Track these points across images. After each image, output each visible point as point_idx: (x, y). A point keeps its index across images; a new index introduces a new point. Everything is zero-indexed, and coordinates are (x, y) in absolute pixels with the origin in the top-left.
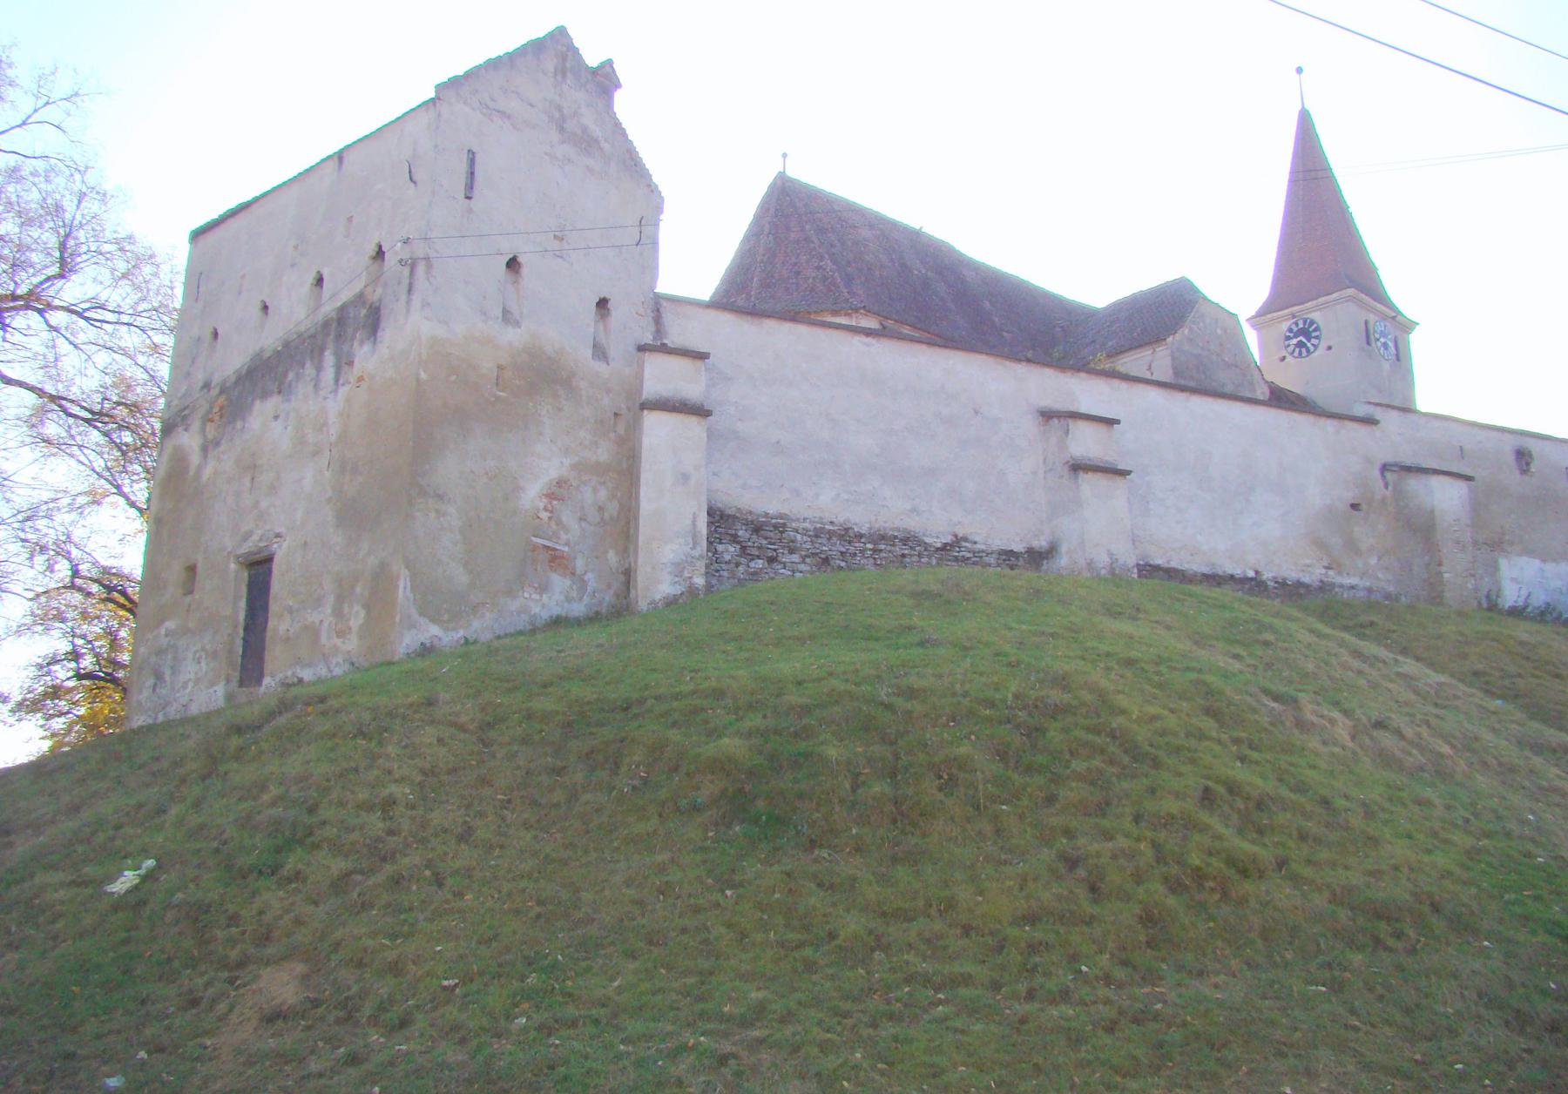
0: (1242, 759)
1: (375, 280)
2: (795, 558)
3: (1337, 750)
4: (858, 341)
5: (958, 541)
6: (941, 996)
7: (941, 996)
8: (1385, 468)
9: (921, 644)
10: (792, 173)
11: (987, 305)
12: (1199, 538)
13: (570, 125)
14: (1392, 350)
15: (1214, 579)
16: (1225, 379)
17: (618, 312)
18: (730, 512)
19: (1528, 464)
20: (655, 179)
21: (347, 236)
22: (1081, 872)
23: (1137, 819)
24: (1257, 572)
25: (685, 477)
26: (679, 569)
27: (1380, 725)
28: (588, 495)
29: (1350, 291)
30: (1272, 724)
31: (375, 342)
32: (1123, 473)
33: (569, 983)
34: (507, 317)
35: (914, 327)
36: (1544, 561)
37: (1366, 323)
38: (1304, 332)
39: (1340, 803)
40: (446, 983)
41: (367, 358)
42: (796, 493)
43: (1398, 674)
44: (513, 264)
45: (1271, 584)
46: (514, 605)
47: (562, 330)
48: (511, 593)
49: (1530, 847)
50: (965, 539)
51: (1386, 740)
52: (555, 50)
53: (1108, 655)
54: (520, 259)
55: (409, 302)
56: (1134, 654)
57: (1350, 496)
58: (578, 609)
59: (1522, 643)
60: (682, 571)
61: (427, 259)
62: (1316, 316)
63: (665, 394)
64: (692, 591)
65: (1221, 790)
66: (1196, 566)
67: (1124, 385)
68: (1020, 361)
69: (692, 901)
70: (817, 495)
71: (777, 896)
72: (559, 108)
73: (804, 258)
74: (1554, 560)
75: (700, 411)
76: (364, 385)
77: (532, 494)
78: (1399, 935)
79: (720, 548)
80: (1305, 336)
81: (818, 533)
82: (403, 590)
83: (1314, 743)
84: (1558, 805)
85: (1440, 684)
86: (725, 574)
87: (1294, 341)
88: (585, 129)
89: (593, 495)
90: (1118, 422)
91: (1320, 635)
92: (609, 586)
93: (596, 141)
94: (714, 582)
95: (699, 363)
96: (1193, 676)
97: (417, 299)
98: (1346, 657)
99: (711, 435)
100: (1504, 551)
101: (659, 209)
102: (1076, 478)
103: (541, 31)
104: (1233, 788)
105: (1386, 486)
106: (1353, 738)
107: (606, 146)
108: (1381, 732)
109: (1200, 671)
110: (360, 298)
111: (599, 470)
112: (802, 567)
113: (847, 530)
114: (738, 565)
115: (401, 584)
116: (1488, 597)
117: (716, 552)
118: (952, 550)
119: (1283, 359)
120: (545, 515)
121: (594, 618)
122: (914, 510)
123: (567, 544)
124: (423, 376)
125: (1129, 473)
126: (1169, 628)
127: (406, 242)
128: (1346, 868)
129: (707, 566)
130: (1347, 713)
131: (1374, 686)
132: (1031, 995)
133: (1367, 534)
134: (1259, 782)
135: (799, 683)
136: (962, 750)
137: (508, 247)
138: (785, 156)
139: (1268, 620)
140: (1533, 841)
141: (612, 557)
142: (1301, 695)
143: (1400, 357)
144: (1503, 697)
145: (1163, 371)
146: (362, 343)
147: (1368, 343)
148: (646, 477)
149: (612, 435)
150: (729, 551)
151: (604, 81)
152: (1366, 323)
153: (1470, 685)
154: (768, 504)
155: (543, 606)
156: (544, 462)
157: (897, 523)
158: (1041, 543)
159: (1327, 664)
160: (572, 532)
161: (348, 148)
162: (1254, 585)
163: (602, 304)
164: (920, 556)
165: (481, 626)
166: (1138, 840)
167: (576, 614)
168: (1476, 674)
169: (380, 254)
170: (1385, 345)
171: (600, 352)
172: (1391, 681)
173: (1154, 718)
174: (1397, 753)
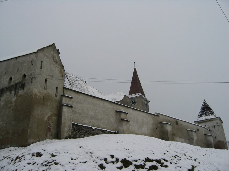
1: (23, 80)
21: (18, 71)
26: (67, 132)
34: (45, 89)
44: (46, 80)
47: (52, 92)
54: (47, 79)
61: (35, 78)
88: (56, 60)
110: (20, 82)
143: (147, 106)
163: (57, 88)
169: (25, 76)
171: (56, 96)
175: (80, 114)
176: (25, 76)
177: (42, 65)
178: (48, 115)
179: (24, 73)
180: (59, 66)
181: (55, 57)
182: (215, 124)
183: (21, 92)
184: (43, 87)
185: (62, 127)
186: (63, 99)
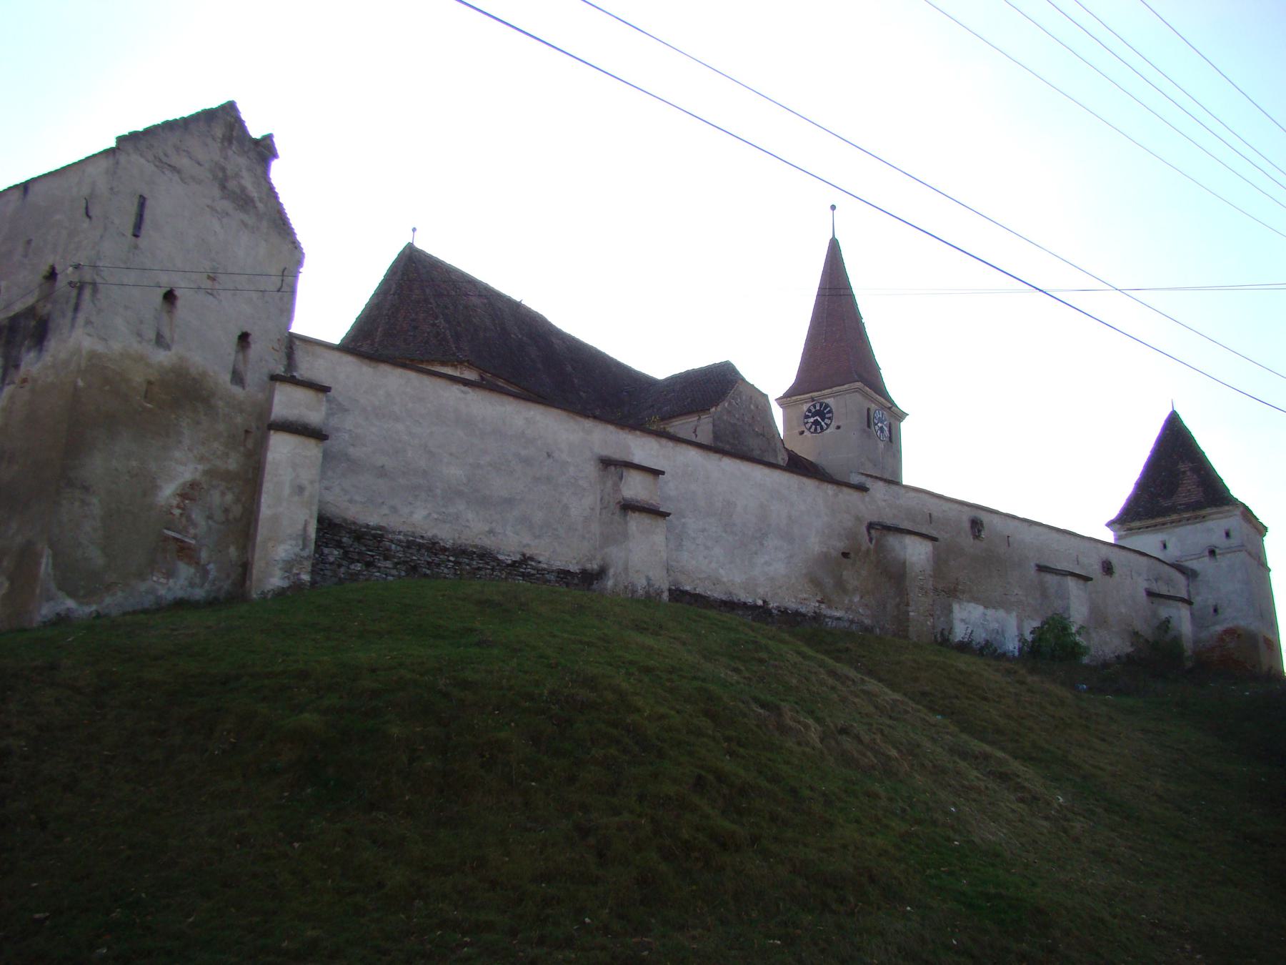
0: (732, 753)
1: (47, 296)
2: (388, 564)
3: (807, 750)
4: (455, 391)
5: (525, 559)
6: (467, 939)
7: (467, 939)
8: (871, 526)
9: (479, 644)
10: (419, 245)
11: (569, 368)
12: (721, 571)
13: (232, 185)
14: (887, 433)
15: (730, 605)
17: (256, 348)
18: (337, 521)
19: (979, 531)
20: (299, 238)
21: (26, 256)
22: (592, 840)
23: (641, 798)
24: (764, 602)
25: (300, 489)
26: (288, 566)
27: (844, 731)
28: (216, 498)
29: (859, 384)
30: (757, 726)
31: (40, 350)
32: (664, 515)
33: (149, 918)
34: (160, 341)
35: (507, 381)
36: (986, 607)
38: (820, 413)
39: (806, 793)
40: (37, 916)
41: (32, 364)
42: (394, 509)
43: (863, 691)
44: (170, 297)
45: (775, 612)
46: (143, 587)
48: (141, 576)
49: (951, 834)
50: (531, 559)
51: (848, 744)
52: (223, 122)
53: (631, 663)
54: (177, 293)
55: (74, 319)
56: (651, 663)
57: (841, 545)
58: (199, 593)
59: (961, 672)
60: (291, 568)
61: (94, 284)
62: (830, 401)
63: (291, 418)
64: (297, 587)
65: (711, 777)
66: (717, 593)
67: (671, 444)
68: (587, 417)
69: (265, 851)
70: (412, 513)
71: (338, 849)
72: (223, 169)
73: (422, 316)
74: (994, 608)
75: (317, 434)
76: (28, 386)
77: (168, 492)
78: (842, 900)
79: (326, 551)
80: (820, 416)
81: (409, 545)
82: (45, 565)
83: (790, 743)
84: (975, 800)
85: (895, 701)
86: (328, 573)
87: (812, 420)
88: (243, 189)
89: (219, 498)
90: (663, 473)
91: (804, 656)
92: (228, 576)
93: (252, 201)
94: (318, 579)
95: (321, 395)
96: (697, 684)
97: (81, 317)
98: (823, 675)
99: (327, 456)
100: (956, 597)
101: (299, 262)
102: (625, 515)
103: (214, 103)
104: (720, 777)
105: (871, 540)
106: (822, 741)
107: (259, 205)
108: (844, 737)
109: (704, 680)
110: (31, 312)
111: (227, 476)
112: (394, 572)
113: (434, 544)
114: (340, 566)
115: (44, 561)
116: (942, 634)
117: (322, 554)
118: (522, 566)
119: (802, 433)
120: (177, 512)
121: (212, 603)
122: (491, 532)
123: (195, 537)
124: (81, 383)
125: (668, 514)
126: (684, 644)
127: (77, 267)
128: (805, 845)
129: (313, 565)
130: (819, 720)
131: (843, 700)
132: (541, 941)
133: (852, 578)
134: (742, 772)
135: (374, 671)
136: (502, 735)
137: (166, 281)
139: (764, 641)
140: (952, 827)
141: (233, 551)
142: (783, 704)
143: (893, 441)
144: (943, 713)
145: (705, 436)
146: (29, 350)
147: (869, 426)
148: (268, 486)
149: (242, 449)
150: (334, 554)
151: (264, 150)
153: (918, 703)
154: (373, 518)
155: (169, 589)
156: (180, 469)
157: (477, 542)
158: (594, 566)
159: (807, 679)
160: (200, 527)
161: (33, 180)
162: (761, 613)
163: (244, 338)
164: (493, 569)
165: (113, 602)
166: (640, 816)
167: (197, 597)
168: (924, 694)
169: (52, 275)
170: (881, 429)
171: (238, 378)
172: (857, 696)
173: (662, 717)
174: (856, 754)
176: (52, 275)
178: (181, 481)
180: (265, 223)
181: (237, 176)
182: (1217, 539)
185: (259, 539)
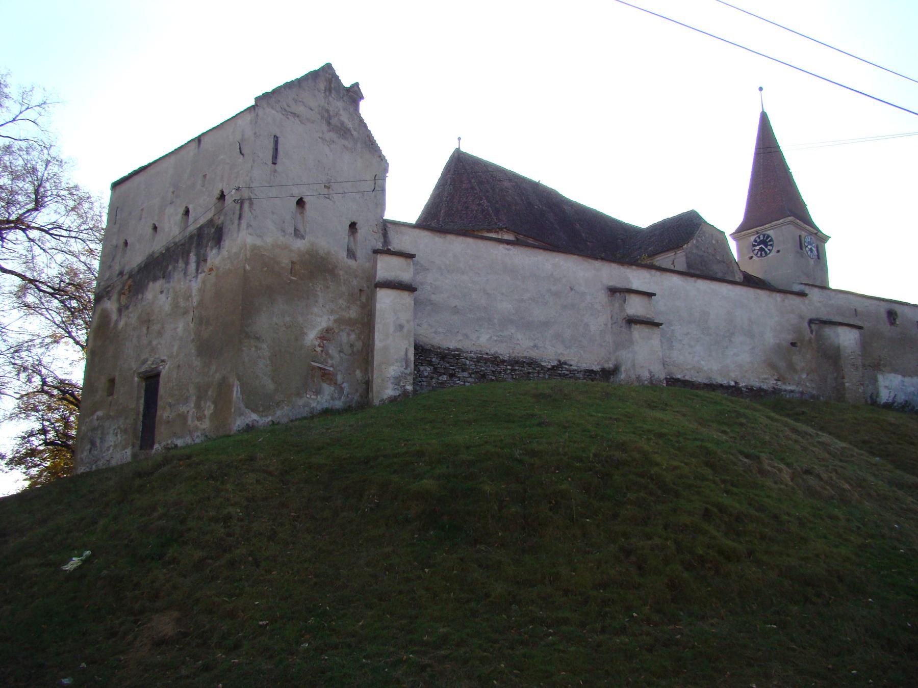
1: (219, 211)
10: (464, 149)
16: (717, 269)
26: (397, 380)
29: (791, 218)
34: (297, 233)
37: (800, 236)
38: (764, 242)
44: (301, 203)
47: (328, 239)
54: (305, 199)
57: (790, 337)
62: (771, 233)
88: (342, 123)
119: (751, 258)
138: (459, 139)
152: (800, 236)
163: (353, 226)
175: (456, 310)
176: (222, 196)
177: (276, 150)
178: (320, 328)
179: (220, 187)
180: (359, 145)
183: (215, 258)
184: (291, 230)
186: (379, 262)
